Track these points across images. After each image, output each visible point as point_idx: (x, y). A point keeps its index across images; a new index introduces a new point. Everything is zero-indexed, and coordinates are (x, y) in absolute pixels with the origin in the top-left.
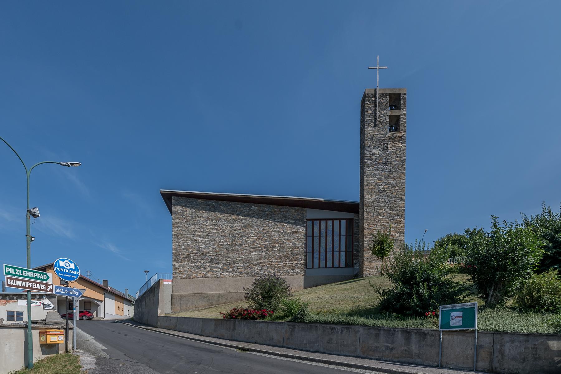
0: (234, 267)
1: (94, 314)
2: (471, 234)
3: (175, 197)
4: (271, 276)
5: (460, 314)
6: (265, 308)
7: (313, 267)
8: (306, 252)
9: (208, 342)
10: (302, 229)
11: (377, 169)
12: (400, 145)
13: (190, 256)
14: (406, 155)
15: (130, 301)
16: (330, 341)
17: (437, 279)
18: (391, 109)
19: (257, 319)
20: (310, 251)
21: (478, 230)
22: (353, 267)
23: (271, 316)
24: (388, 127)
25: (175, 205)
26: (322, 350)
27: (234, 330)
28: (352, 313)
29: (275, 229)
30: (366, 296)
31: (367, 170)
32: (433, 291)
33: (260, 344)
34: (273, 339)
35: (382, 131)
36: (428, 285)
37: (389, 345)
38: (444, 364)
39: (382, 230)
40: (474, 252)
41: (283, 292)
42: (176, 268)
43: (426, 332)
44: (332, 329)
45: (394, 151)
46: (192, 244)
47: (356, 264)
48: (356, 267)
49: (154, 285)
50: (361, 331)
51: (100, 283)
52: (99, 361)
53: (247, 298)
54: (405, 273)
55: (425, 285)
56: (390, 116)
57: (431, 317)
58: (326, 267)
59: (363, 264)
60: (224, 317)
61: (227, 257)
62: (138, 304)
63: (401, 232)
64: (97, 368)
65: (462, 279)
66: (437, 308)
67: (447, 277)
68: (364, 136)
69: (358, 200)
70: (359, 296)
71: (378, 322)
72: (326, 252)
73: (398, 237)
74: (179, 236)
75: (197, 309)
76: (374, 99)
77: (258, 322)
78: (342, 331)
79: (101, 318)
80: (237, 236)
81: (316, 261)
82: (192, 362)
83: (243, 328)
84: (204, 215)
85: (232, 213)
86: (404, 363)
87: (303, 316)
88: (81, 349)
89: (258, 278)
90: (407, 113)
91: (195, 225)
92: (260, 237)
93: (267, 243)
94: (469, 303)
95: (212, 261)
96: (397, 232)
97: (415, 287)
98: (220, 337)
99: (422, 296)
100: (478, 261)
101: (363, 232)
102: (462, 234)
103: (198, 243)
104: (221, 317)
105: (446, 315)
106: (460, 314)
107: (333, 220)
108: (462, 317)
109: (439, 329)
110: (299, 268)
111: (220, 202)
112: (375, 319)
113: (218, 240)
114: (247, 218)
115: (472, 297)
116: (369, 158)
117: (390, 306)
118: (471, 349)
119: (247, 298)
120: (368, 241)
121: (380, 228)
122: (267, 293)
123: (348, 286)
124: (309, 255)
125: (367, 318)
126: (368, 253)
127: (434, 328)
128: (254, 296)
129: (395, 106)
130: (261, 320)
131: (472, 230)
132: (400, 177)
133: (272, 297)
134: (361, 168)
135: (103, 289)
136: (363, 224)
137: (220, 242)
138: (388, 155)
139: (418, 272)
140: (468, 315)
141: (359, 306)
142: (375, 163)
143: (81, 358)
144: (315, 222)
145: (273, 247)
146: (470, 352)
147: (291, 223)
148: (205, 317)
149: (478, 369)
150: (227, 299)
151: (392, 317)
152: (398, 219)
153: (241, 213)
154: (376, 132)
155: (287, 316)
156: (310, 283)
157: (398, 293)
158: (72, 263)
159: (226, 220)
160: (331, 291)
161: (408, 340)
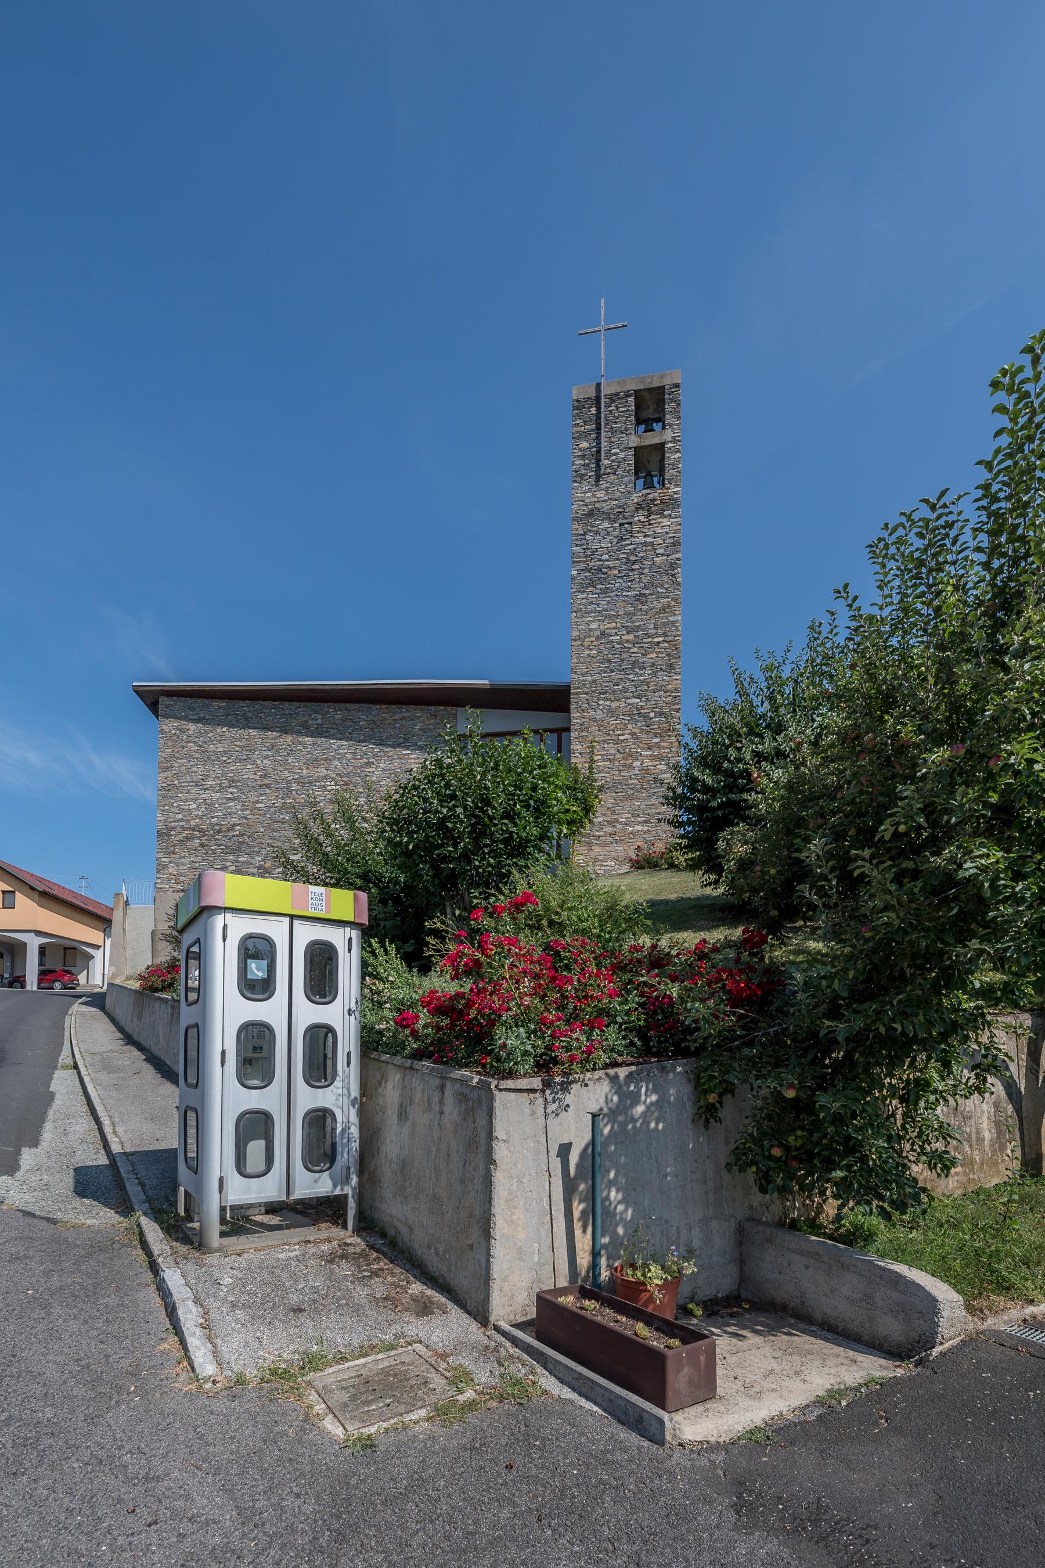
1: (82, 978)
11: (604, 592)
12: (666, 522)
13: (193, 838)
42: (165, 867)
45: (649, 540)
46: (197, 809)
56: (638, 451)
76: (593, 410)
84: (225, 738)
91: (206, 761)
95: (239, 850)
103: (209, 805)
111: (258, 705)
114: (319, 740)
116: (583, 566)
121: (612, 752)
132: (666, 609)
137: (257, 802)
138: (632, 552)
153: (305, 729)
159: (270, 748)
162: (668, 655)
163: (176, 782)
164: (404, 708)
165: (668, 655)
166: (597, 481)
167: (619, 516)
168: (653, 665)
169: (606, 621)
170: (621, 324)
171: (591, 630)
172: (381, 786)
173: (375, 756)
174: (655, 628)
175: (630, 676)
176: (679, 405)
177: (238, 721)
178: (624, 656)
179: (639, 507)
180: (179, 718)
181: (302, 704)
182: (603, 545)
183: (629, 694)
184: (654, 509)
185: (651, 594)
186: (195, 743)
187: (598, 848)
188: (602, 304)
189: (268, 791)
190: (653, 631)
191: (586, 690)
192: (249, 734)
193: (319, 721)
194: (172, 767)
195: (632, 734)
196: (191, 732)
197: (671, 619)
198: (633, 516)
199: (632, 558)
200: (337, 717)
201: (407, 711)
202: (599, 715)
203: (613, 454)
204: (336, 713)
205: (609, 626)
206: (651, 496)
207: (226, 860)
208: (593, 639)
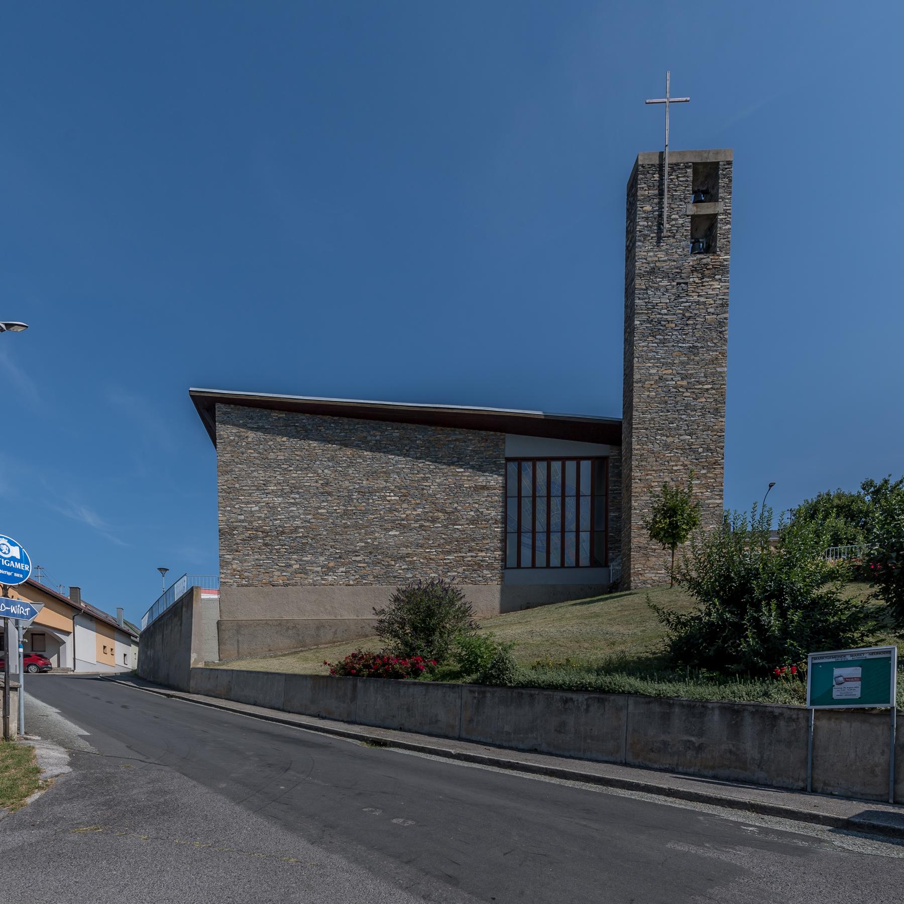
0: (350, 563)
1: (53, 661)
2: (877, 492)
3: (222, 406)
4: (432, 584)
5: (857, 672)
6: (419, 653)
7: (519, 566)
8: (505, 532)
9: (300, 725)
10: (495, 480)
12: (716, 285)
13: (257, 537)
14: (729, 309)
15: (129, 635)
16: (561, 728)
17: (801, 594)
18: (697, 201)
19: (402, 677)
20: (513, 531)
21: (892, 482)
22: (607, 566)
23: (432, 671)
24: (687, 243)
25: (223, 423)
26: (544, 747)
27: (354, 699)
28: (609, 668)
29: (438, 479)
30: (638, 631)
31: (640, 346)
32: (792, 621)
33: (410, 731)
34: (437, 721)
35: (675, 252)
36: (779, 606)
37: (693, 739)
38: (819, 786)
39: (672, 484)
40: (888, 532)
41: (459, 619)
42: (228, 563)
43: (777, 712)
44: (566, 701)
45: (702, 299)
47: (613, 559)
48: (614, 566)
49: (181, 600)
50: (631, 708)
51: (66, 595)
52: (76, 758)
53: (382, 630)
54: (728, 578)
55: (773, 606)
56: (694, 218)
57: (787, 679)
58: (548, 566)
59: (629, 560)
60: (333, 672)
61: (335, 541)
62: (146, 641)
63: (717, 489)
64: (74, 774)
65: (859, 594)
66: (801, 659)
67: (824, 590)
68: (634, 266)
69: (617, 414)
70: (622, 630)
71: (666, 688)
72: (548, 532)
73: (708, 498)
74: (231, 492)
75: (272, 653)
76: (656, 176)
77: (405, 684)
78: (588, 706)
79: (68, 670)
80: (355, 495)
81: (526, 553)
82: (270, 765)
83: (374, 697)
84: (284, 447)
85: (345, 444)
86: (727, 780)
87: (502, 671)
88: (36, 734)
89: (404, 588)
90: (732, 207)
92: (404, 498)
93: (420, 511)
94: (874, 648)
95: (303, 550)
96: (707, 487)
97: (751, 612)
98: (324, 715)
99: (767, 630)
100: (898, 551)
101: (629, 487)
102: (855, 493)
103: (272, 508)
104: (325, 671)
105: (823, 673)
106: (857, 672)
107: (563, 459)
108: (860, 679)
109: (807, 705)
110: (490, 567)
111: (318, 419)
112: (661, 680)
113: (314, 503)
114: (378, 455)
115: (882, 637)
116: (645, 317)
117: (698, 652)
118: (883, 753)
119: (382, 630)
120: (641, 507)
121: (667, 479)
122: (424, 621)
123: (596, 607)
124: (512, 539)
125: (643, 679)
126: (640, 535)
127: (796, 703)
128: (396, 625)
129: (705, 192)
130: (412, 680)
131: (878, 482)
133: (434, 630)
134: (626, 340)
135: (70, 607)
136: (631, 470)
137: (320, 508)
138: (687, 309)
139: (756, 576)
140: (876, 676)
141: (623, 652)
142: (657, 328)
143: (37, 752)
144: (524, 464)
145: (434, 520)
146: (880, 759)
147: (473, 467)
148: (290, 672)
149: (900, 799)
150: (335, 633)
151: (698, 678)
152: (710, 457)
153: (364, 444)
154: (662, 255)
155: (469, 672)
156: (515, 602)
157: (711, 624)
158: (13, 544)
160: (560, 620)
161: (735, 730)
162: (715, 400)
163: (237, 486)
164: (457, 431)
165: (715, 400)
166: (658, 242)
167: (675, 275)
168: (703, 408)
169: (664, 368)
170: (684, 99)
171: (650, 375)
172: (437, 499)
173: (431, 472)
174: (705, 377)
175: (683, 417)
176: (730, 181)
177: (298, 432)
178: (678, 399)
179: (694, 270)
180: (237, 426)
181: (361, 421)
182: (662, 301)
183: (682, 432)
184: (707, 272)
185: (702, 347)
186: (255, 450)
187: (654, 559)
188: (668, 78)
189: (330, 498)
190: (703, 379)
191: (646, 426)
192: (310, 444)
193: (378, 438)
194: (232, 471)
195: (684, 465)
196: (250, 440)
197: (719, 370)
198: (689, 277)
199: (687, 314)
200: (395, 435)
201: (460, 434)
202: (657, 448)
203: (673, 220)
204: (395, 432)
205: (666, 372)
206: (704, 261)
207: (290, 559)
208: (653, 382)
